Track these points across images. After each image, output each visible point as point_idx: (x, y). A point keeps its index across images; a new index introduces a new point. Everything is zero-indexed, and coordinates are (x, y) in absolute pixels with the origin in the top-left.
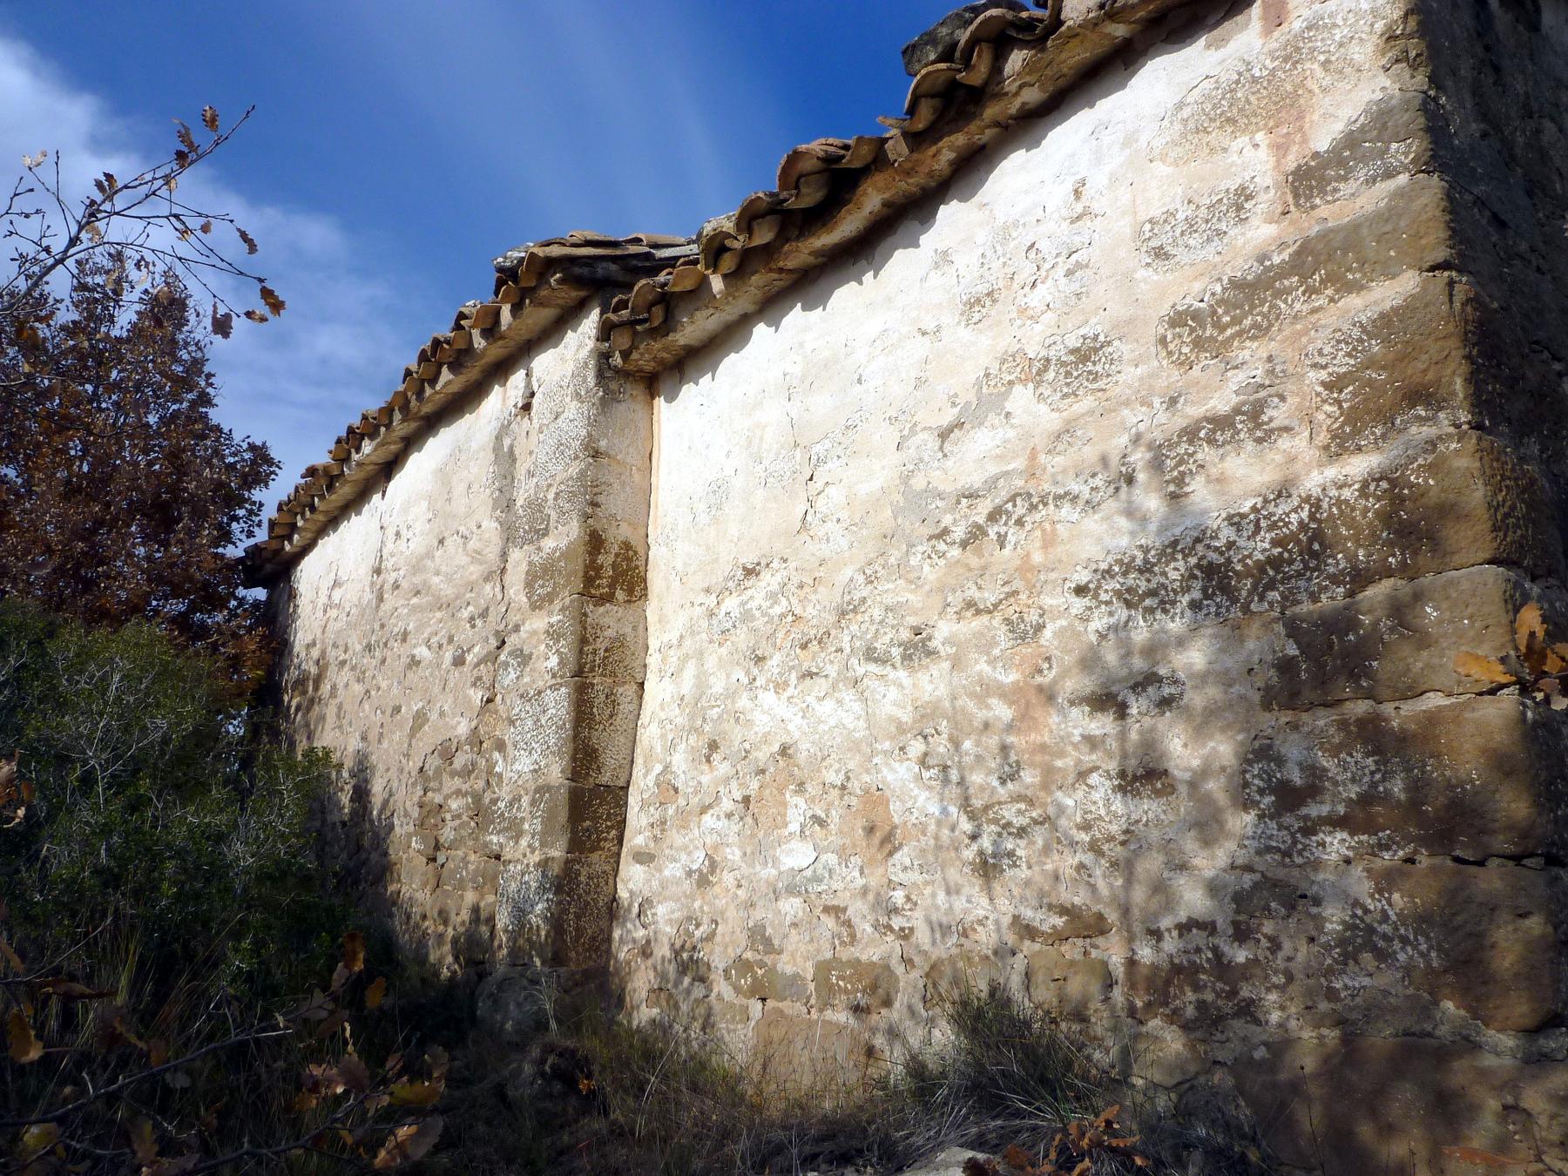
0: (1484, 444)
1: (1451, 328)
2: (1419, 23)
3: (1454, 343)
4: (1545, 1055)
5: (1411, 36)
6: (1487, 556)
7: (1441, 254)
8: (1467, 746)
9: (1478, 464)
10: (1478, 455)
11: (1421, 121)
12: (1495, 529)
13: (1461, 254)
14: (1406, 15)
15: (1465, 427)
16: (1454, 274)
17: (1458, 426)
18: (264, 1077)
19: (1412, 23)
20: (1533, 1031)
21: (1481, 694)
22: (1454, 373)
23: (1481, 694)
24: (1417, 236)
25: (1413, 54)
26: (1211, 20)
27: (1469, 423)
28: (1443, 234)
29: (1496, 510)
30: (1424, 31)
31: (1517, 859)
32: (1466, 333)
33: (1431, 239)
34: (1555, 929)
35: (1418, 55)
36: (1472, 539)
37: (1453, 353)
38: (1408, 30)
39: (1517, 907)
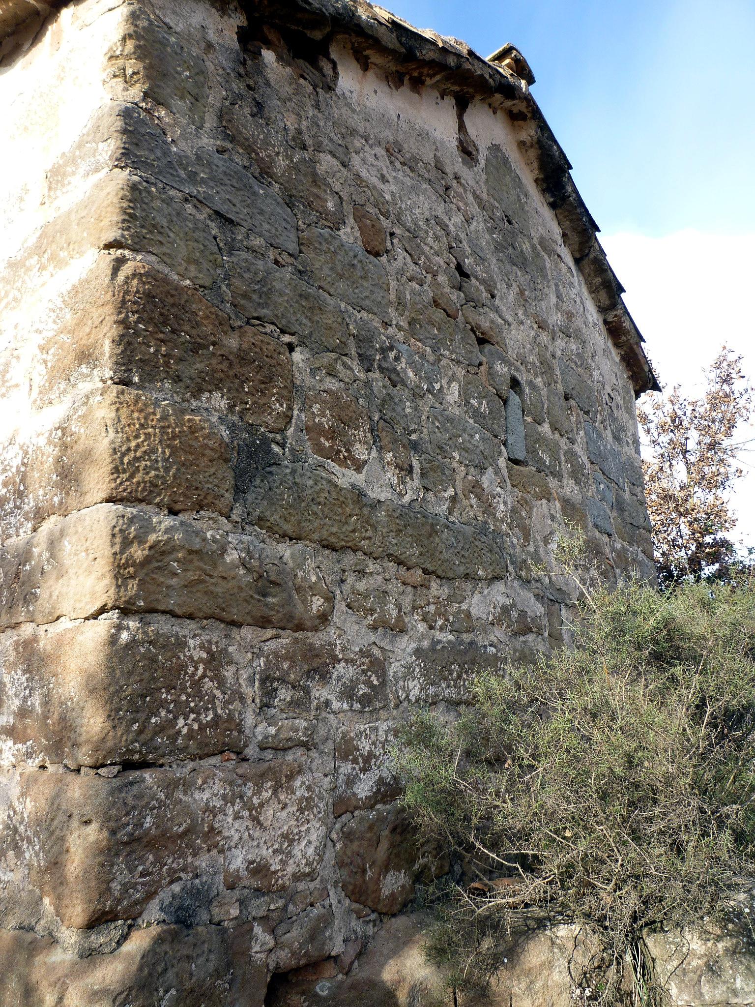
0: (127, 397)
1: (109, 296)
2: (137, 47)
3: (109, 309)
4: (94, 950)
5: (128, 57)
6: (104, 495)
7: (112, 234)
8: (73, 666)
9: (113, 414)
10: (114, 407)
11: (119, 124)
12: (116, 470)
13: (136, 236)
14: (124, 39)
15: (109, 382)
16: (127, 252)
17: (104, 382)
18: (201, 564)
19: (130, 45)
20: (93, 924)
21: (87, 619)
22: (105, 336)
23: (87, 619)
24: (99, 219)
25: (129, 72)
26: (25, 48)
27: (111, 378)
28: (117, 218)
29: (124, 455)
30: (141, 53)
31: (96, 767)
32: (123, 302)
33: (106, 222)
34: (113, 832)
35: (134, 73)
36: (98, 481)
37: (107, 318)
38: (126, 53)
39: (83, 816)
